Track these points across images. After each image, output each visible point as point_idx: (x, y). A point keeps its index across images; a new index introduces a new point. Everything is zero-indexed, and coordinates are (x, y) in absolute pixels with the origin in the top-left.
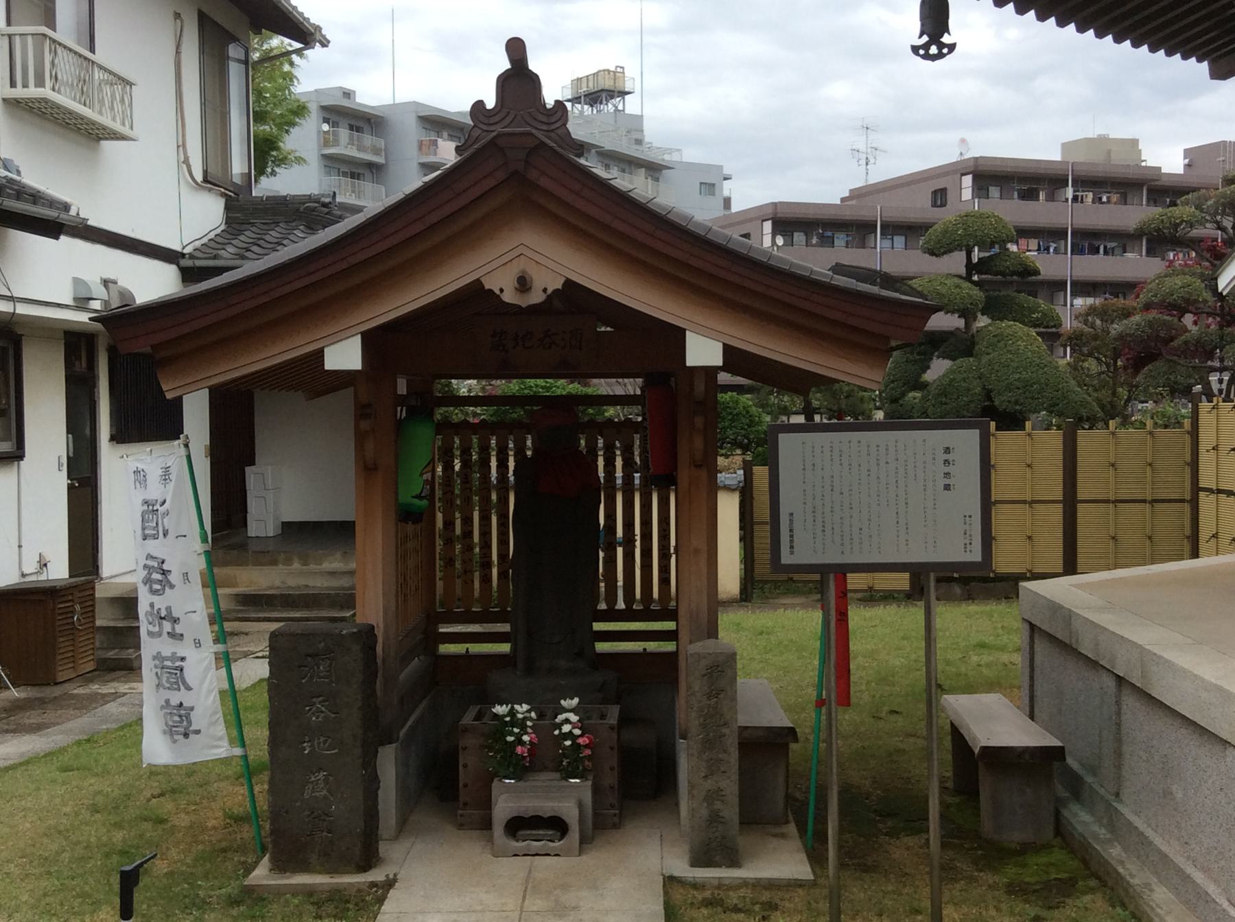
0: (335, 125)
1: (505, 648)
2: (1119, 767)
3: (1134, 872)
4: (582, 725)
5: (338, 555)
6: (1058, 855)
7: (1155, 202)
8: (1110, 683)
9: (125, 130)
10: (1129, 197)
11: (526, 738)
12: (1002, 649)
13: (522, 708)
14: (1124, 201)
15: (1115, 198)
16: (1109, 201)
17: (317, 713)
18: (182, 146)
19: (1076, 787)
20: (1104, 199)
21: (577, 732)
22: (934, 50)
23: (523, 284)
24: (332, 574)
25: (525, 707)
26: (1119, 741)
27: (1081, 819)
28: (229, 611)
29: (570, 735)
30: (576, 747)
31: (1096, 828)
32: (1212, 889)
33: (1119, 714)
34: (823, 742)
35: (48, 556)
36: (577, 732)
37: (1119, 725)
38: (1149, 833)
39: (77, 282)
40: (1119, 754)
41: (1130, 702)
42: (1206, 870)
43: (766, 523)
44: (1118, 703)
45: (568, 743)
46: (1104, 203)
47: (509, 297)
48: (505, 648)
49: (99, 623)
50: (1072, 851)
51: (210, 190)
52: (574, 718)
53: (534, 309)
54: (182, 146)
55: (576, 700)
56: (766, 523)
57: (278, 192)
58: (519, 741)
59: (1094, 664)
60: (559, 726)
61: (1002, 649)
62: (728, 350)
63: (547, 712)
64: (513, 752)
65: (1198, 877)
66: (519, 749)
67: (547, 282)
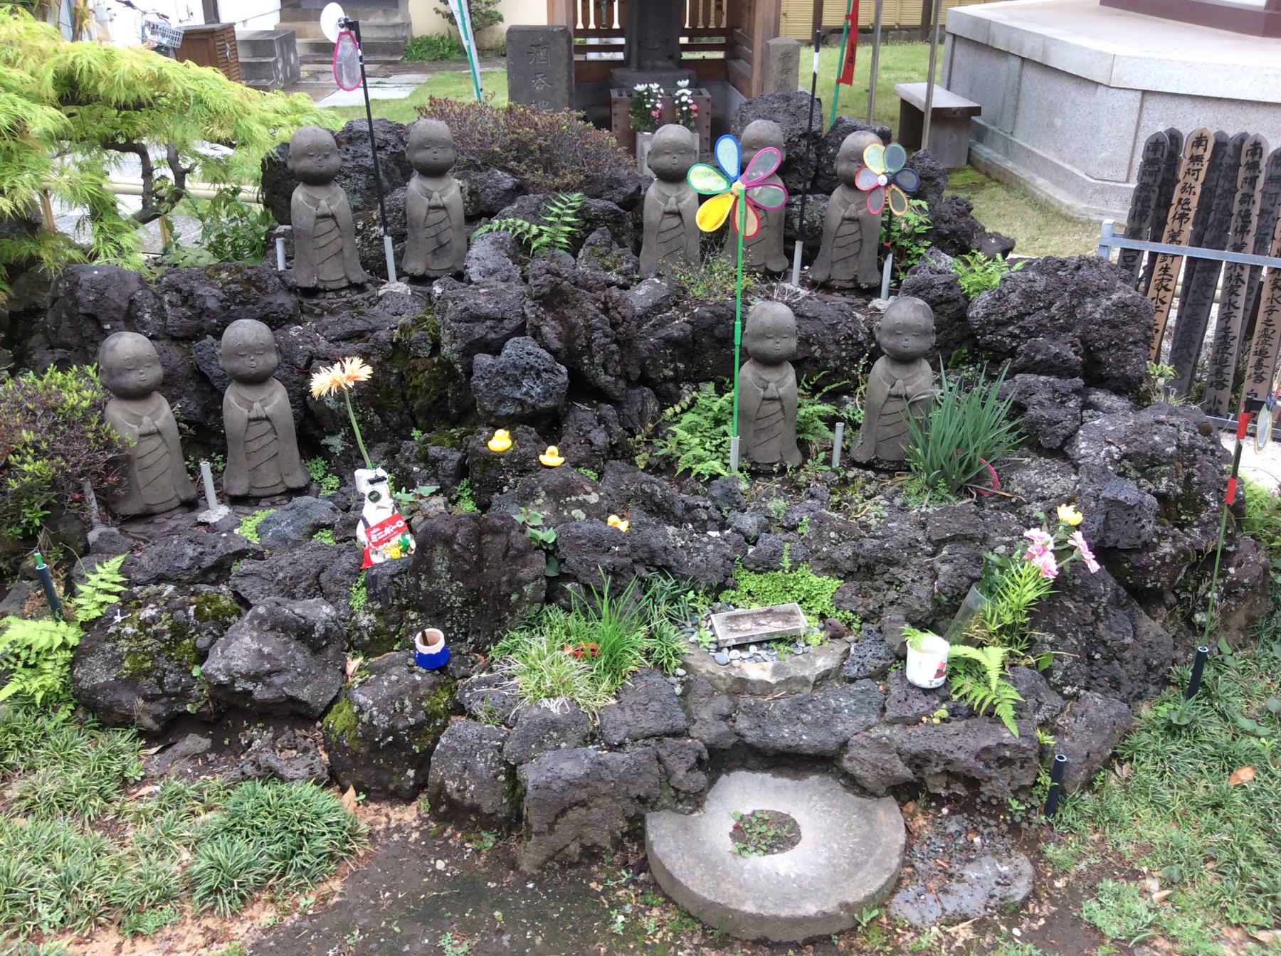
1: (620, 56)
2: (1015, 115)
3: (1022, 172)
4: (691, 97)
5: (380, 12)
6: (970, 173)
8: (1016, 63)
11: (659, 105)
12: (901, 69)
13: (655, 86)
17: (539, 85)
19: (981, 134)
21: (690, 101)
24: (379, 27)
25: (656, 86)
26: (1018, 100)
27: (985, 152)
28: (306, 56)
29: (686, 103)
30: (689, 111)
31: (995, 155)
32: (1076, 171)
33: (1020, 83)
34: (207, 418)
35: (192, 10)
36: (690, 101)
37: (1019, 90)
38: (1034, 149)
40: (1016, 108)
41: (1030, 73)
42: (1072, 162)
44: (1020, 76)
45: (685, 108)
48: (620, 56)
49: (241, 60)
50: (978, 170)
52: (689, 92)
55: (687, 82)
58: (654, 108)
59: (1005, 54)
60: (679, 98)
61: (901, 69)
63: (671, 86)
64: (650, 115)
65: (1067, 166)
66: (654, 113)
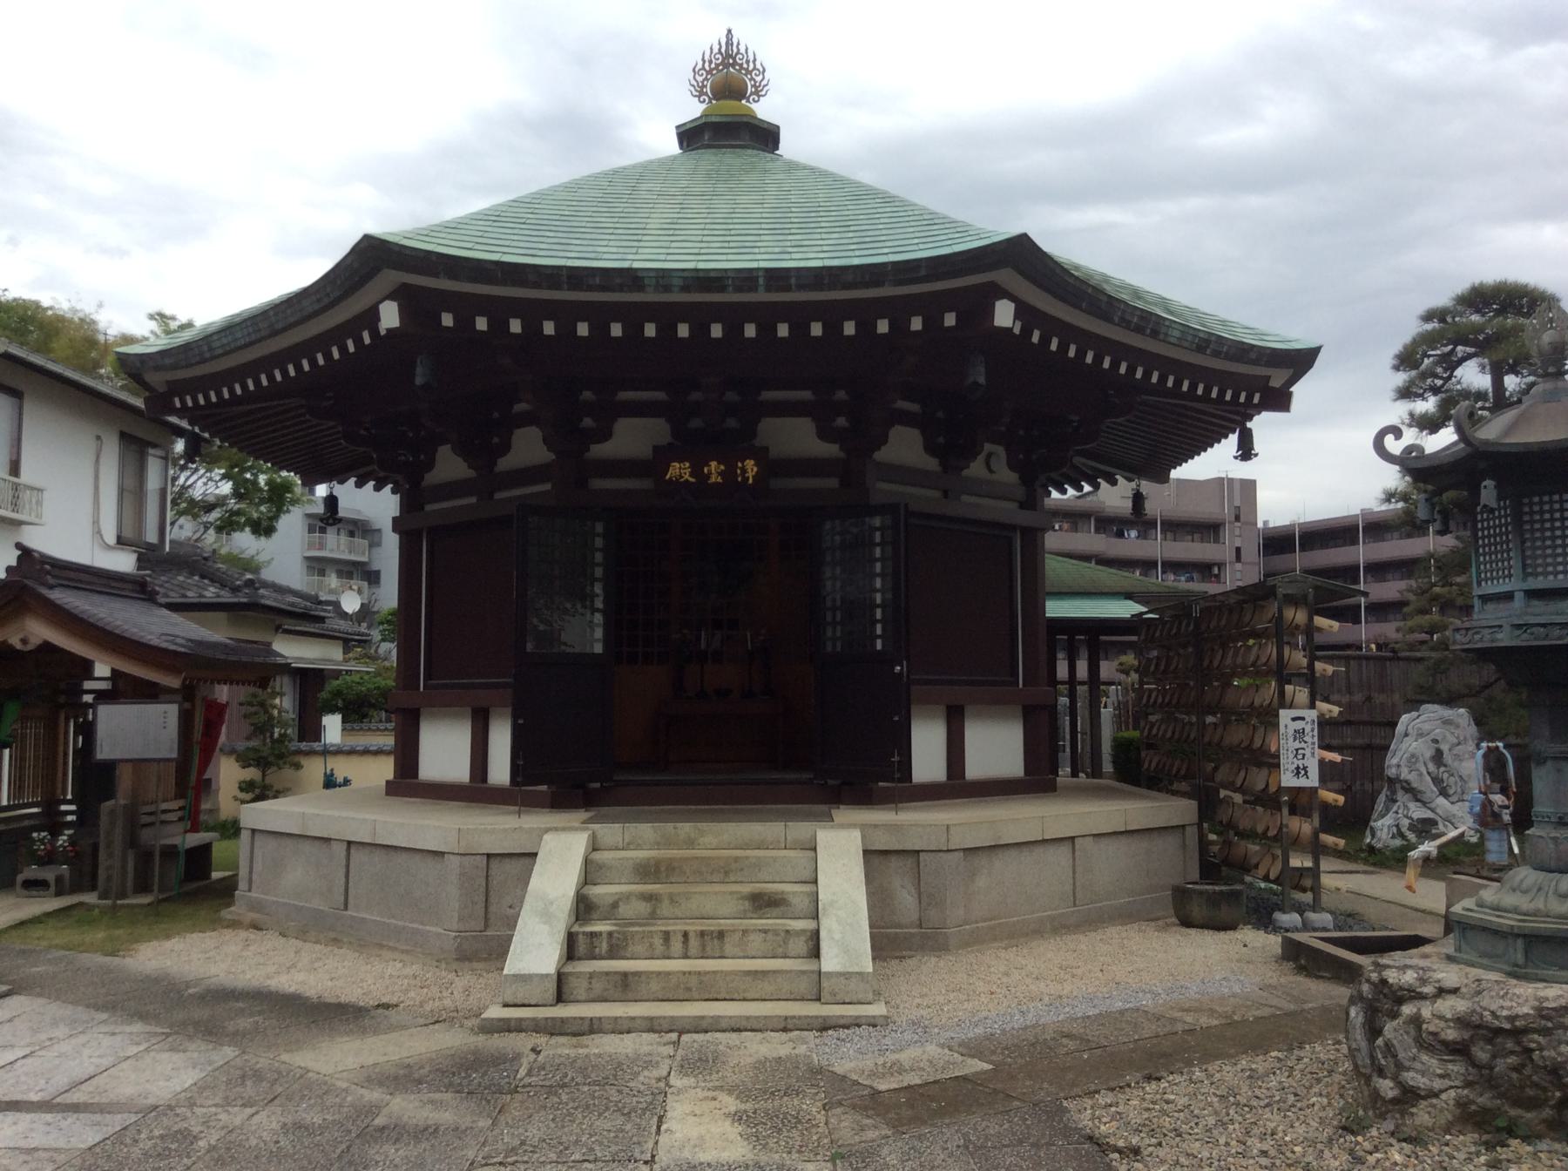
0: (322, 573)
7: (1105, 529)
9: (37, 521)
10: (1080, 525)
13: (43, 834)
14: (1075, 529)
15: (1066, 526)
16: (1061, 529)
18: (96, 522)
20: (1057, 527)
22: (331, 521)
23: (24, 641)
30: (65, 847)
39: (1400, 417)
43: (1325, 872)
46: (1056, 531)
47: (19, 646)
51: (123, 549)
53: (30, 652)
54: (96, 522)
56: (1325, 872)
57: (359, 512)
62: (113, 670)
67: (34, 642)
